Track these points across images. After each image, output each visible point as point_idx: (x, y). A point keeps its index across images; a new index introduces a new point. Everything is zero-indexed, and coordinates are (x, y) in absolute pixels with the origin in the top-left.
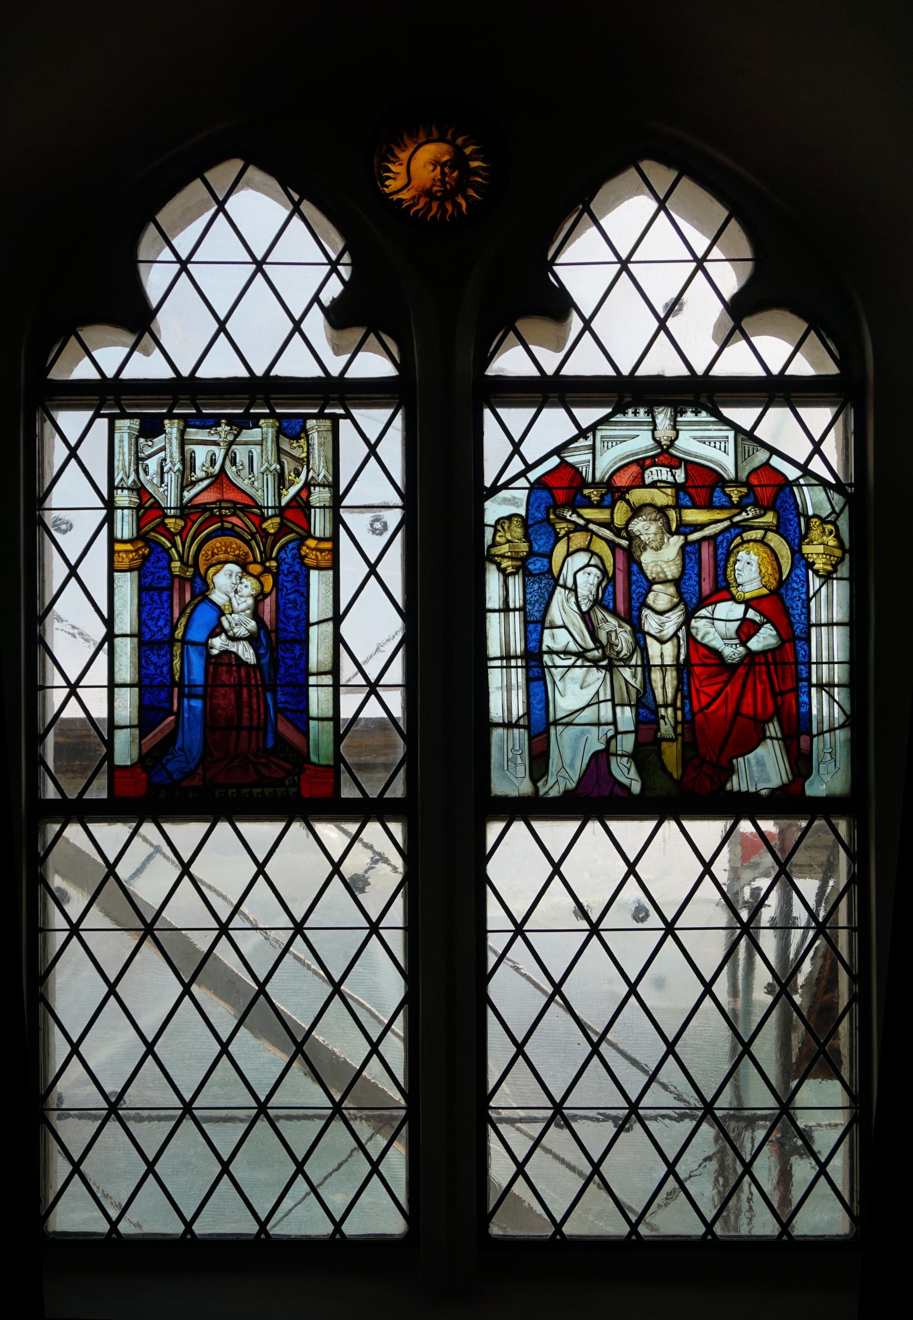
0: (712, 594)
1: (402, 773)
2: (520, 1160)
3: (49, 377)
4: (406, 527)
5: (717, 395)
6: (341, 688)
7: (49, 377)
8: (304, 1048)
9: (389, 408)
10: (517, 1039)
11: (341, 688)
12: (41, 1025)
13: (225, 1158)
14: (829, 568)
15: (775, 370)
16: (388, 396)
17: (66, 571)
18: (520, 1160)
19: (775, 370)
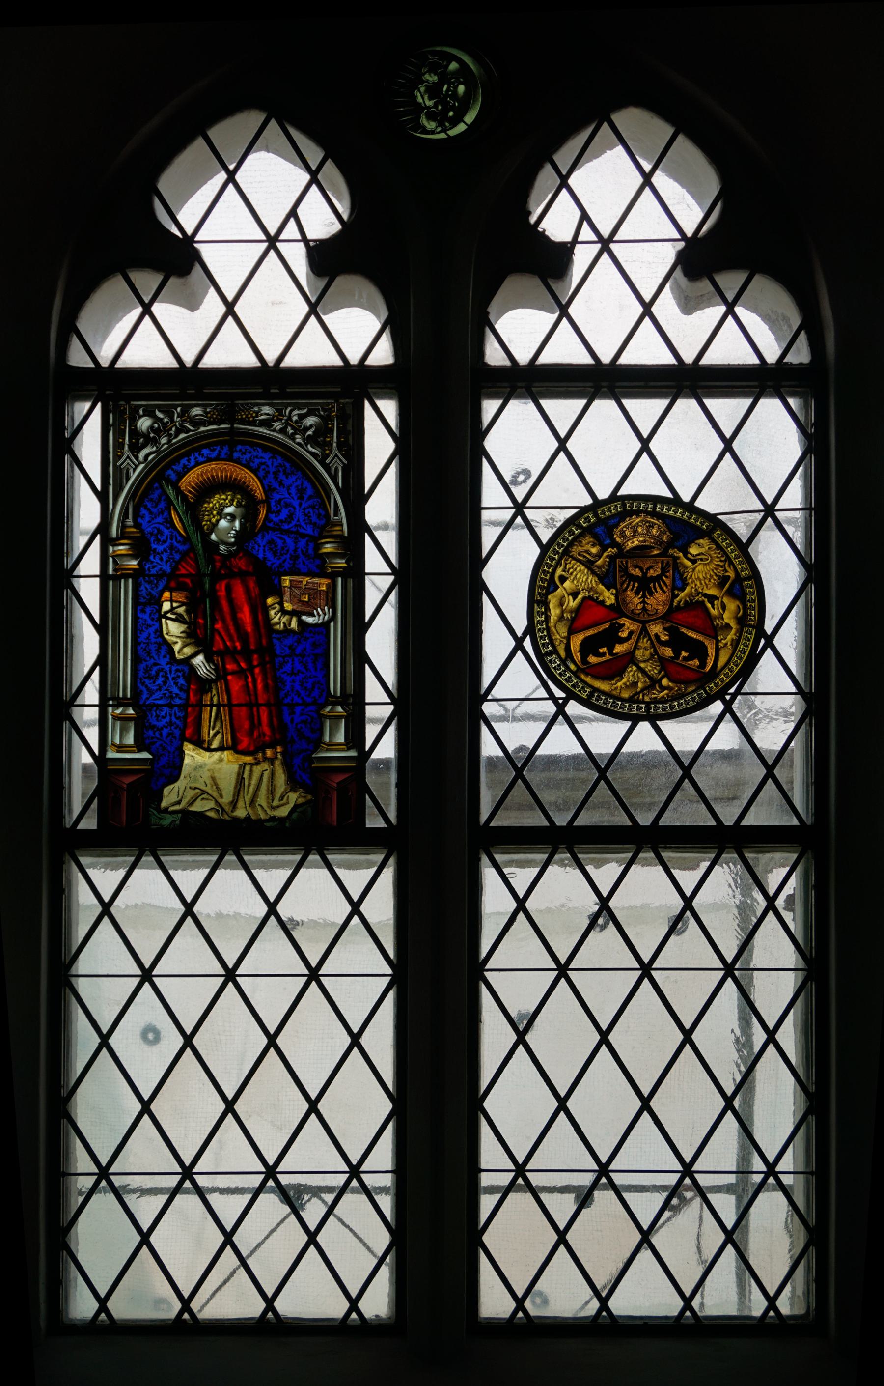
0: (118, 539)
1: (391, 731)
2: (355, 1030)
3: (646, 978)
4: (400, 459)
5: (537, 384)
6: (367, 706)
7: (646, 978)
8: (597, 775)
9: (207, 292)
10: (228, 1096)
11: (367, 706)
12: (813, 1286)
13: (728, 435)
14: (264, 475)
15: (354, 359)
16: (642, 384)
17: (778, 1036)
18: (355, 1030)
19: (354, 359)
